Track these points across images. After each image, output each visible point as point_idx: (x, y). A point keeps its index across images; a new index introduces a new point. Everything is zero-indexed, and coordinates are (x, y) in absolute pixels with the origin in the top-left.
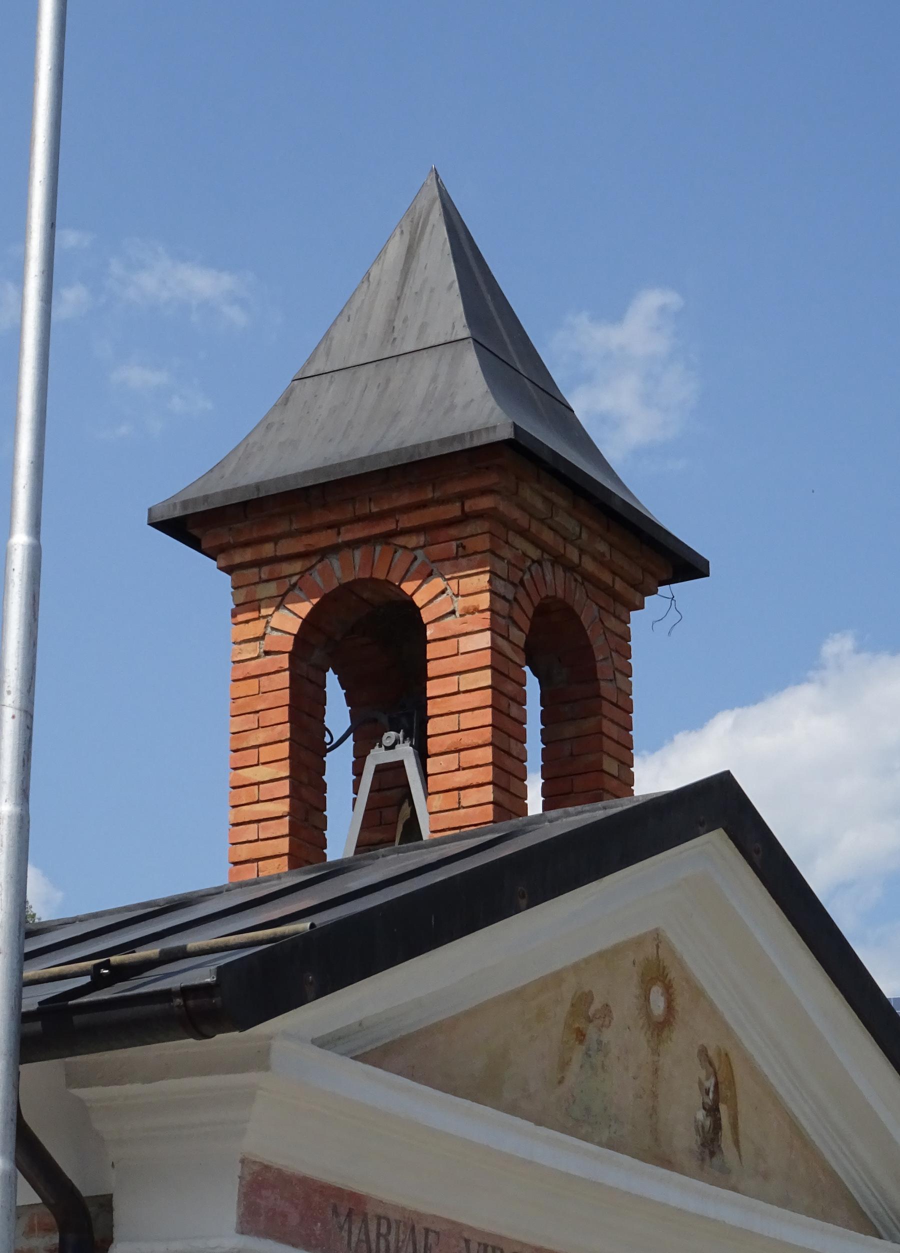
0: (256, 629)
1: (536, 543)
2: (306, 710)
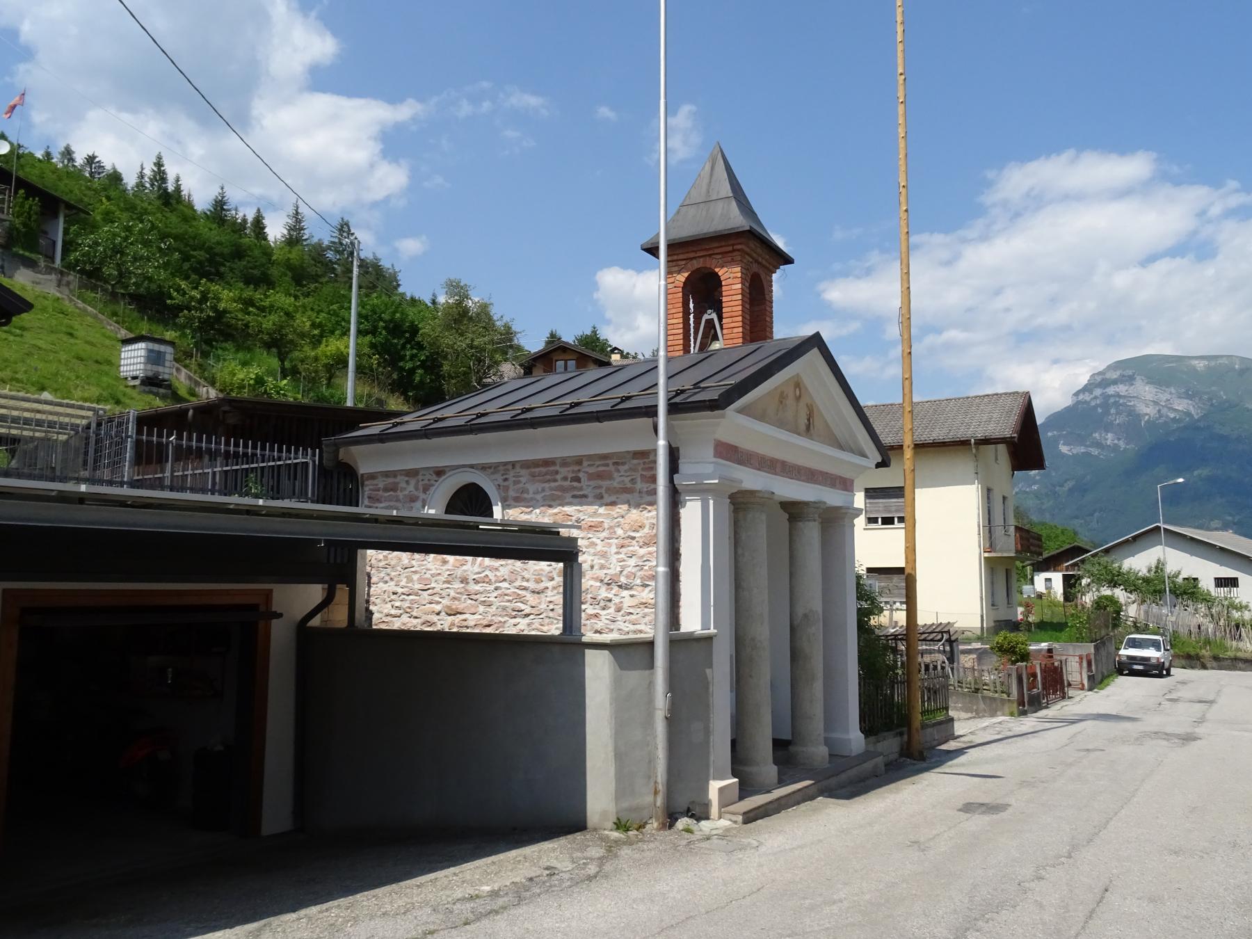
2: (685, 304)
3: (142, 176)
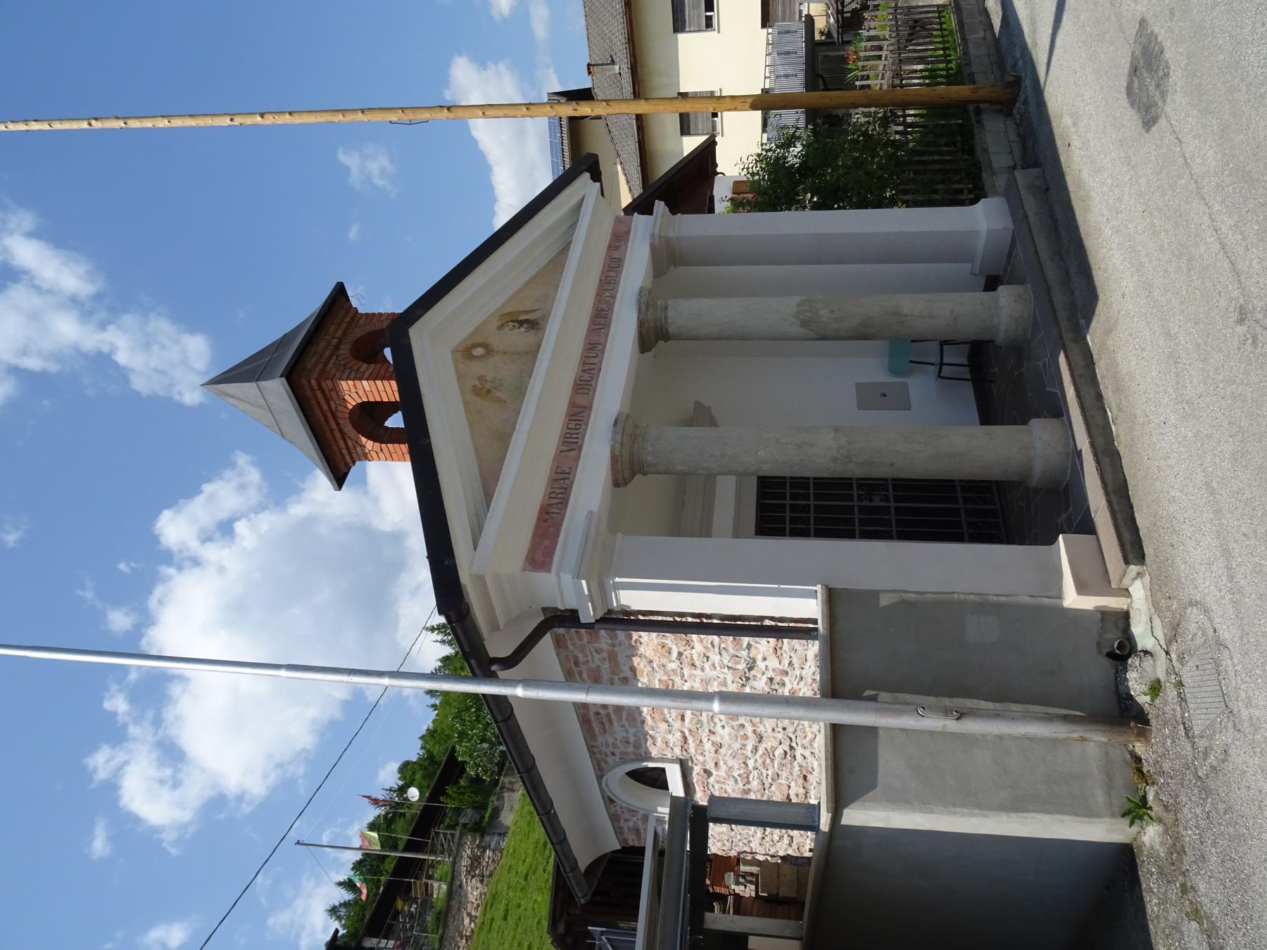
0: (373, 454)
1: (330, 357)
3: (443, 642)
